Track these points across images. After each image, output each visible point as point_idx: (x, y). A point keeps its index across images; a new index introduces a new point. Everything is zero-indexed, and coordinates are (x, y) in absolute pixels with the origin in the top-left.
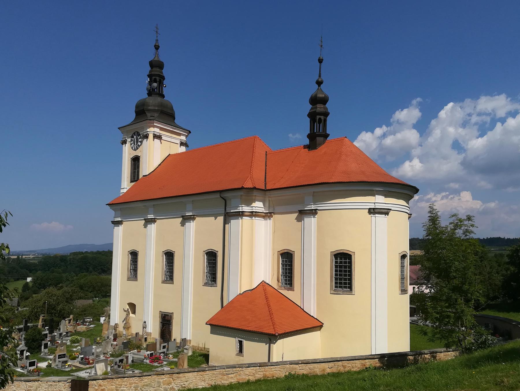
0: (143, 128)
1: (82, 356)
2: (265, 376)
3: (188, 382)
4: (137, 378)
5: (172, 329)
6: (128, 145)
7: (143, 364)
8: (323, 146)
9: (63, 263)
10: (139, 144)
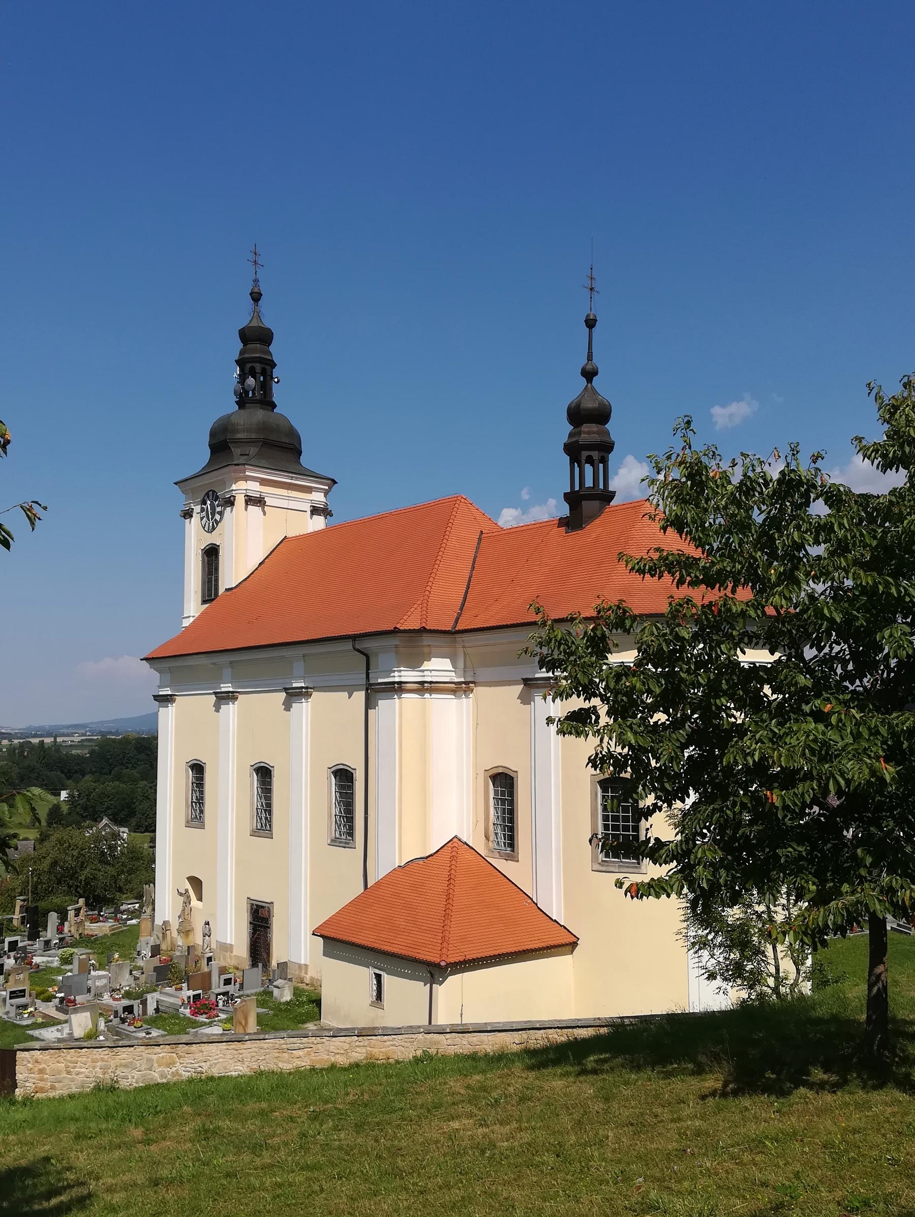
0: (224, 483)
1: (62, 995)
2: (370, 1056)
3: (208, 1063)
4: (107, 1051)
5: (271, 938)
6: (196, 519)
7: (178, 1018)
8: (597, 522)
9: (142, 756)
10: (217, 517)
